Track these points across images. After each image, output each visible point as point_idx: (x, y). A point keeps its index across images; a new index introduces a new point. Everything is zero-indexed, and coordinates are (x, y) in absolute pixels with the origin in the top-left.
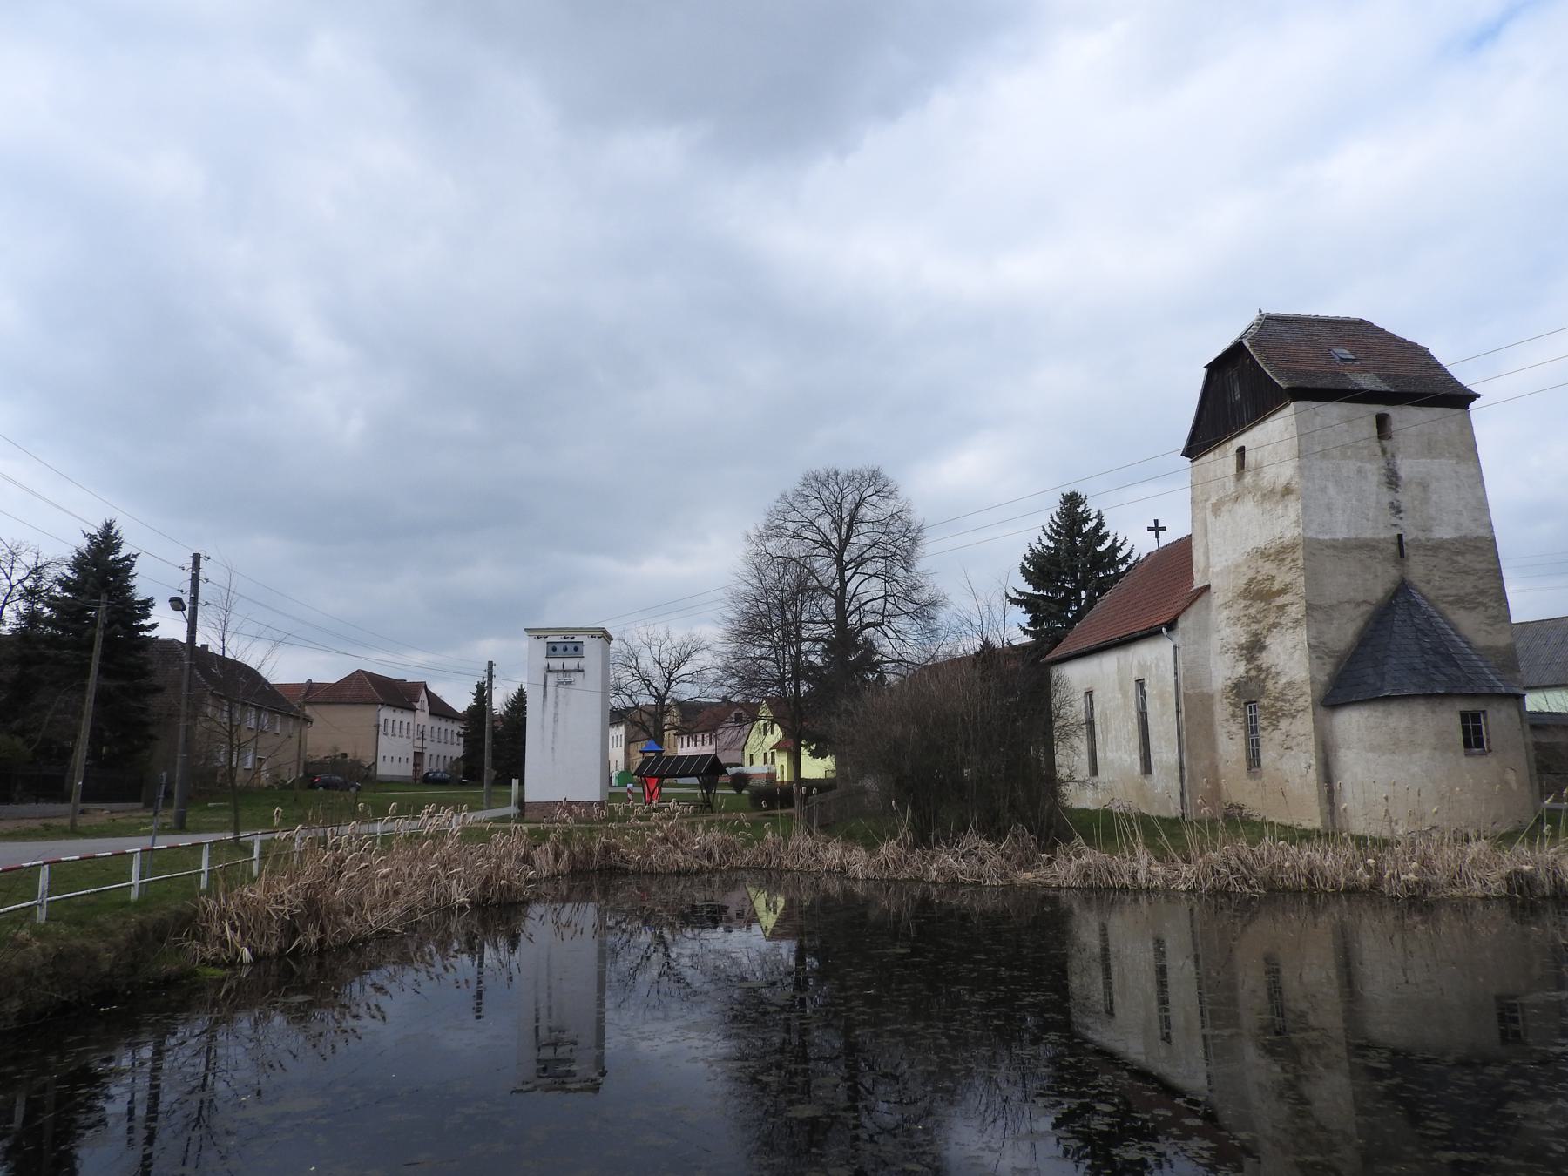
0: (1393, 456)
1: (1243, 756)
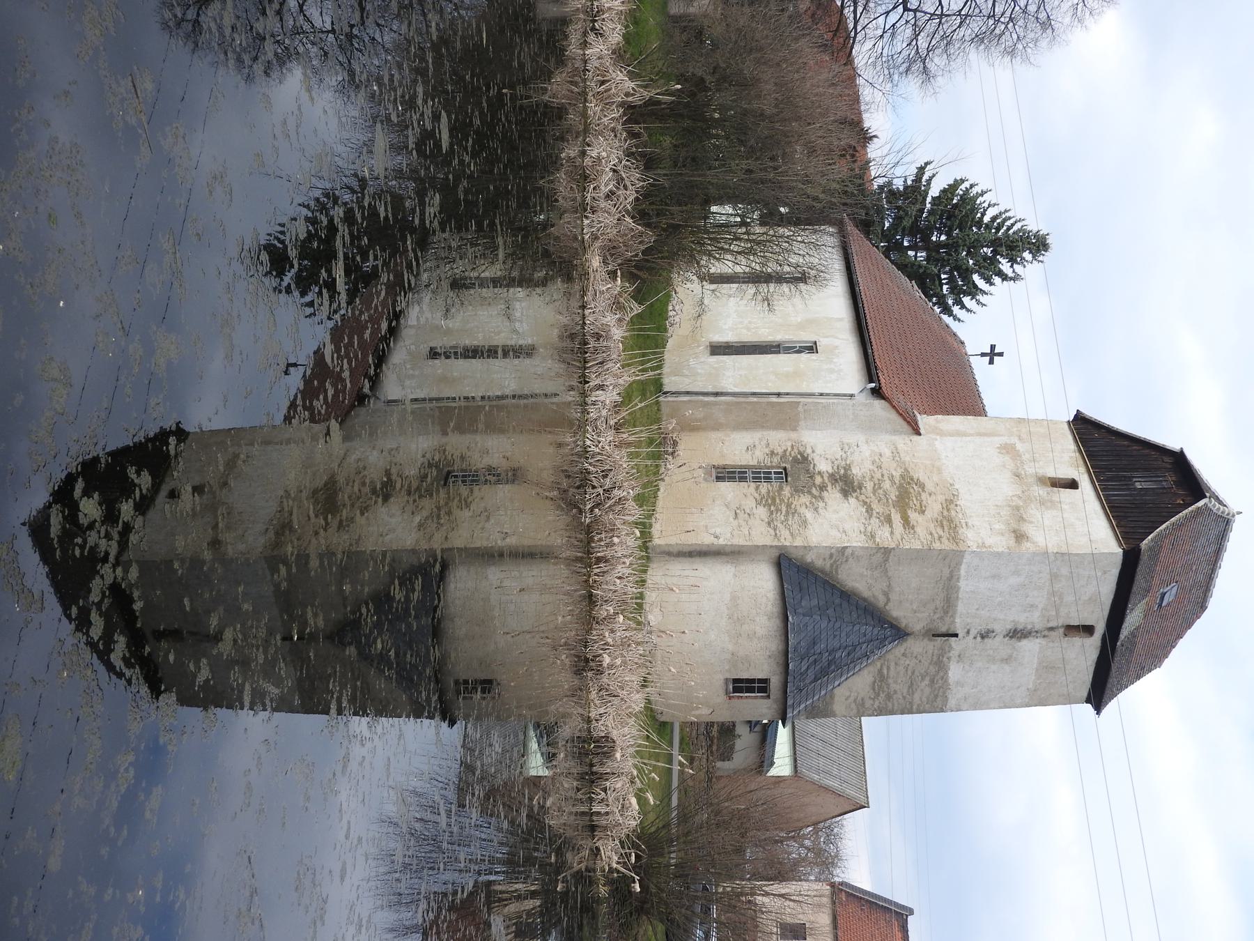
0: (1044, 636)
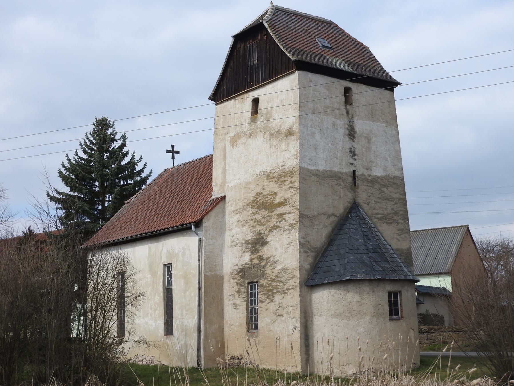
0: (352, 117)
1: (245, 321)
